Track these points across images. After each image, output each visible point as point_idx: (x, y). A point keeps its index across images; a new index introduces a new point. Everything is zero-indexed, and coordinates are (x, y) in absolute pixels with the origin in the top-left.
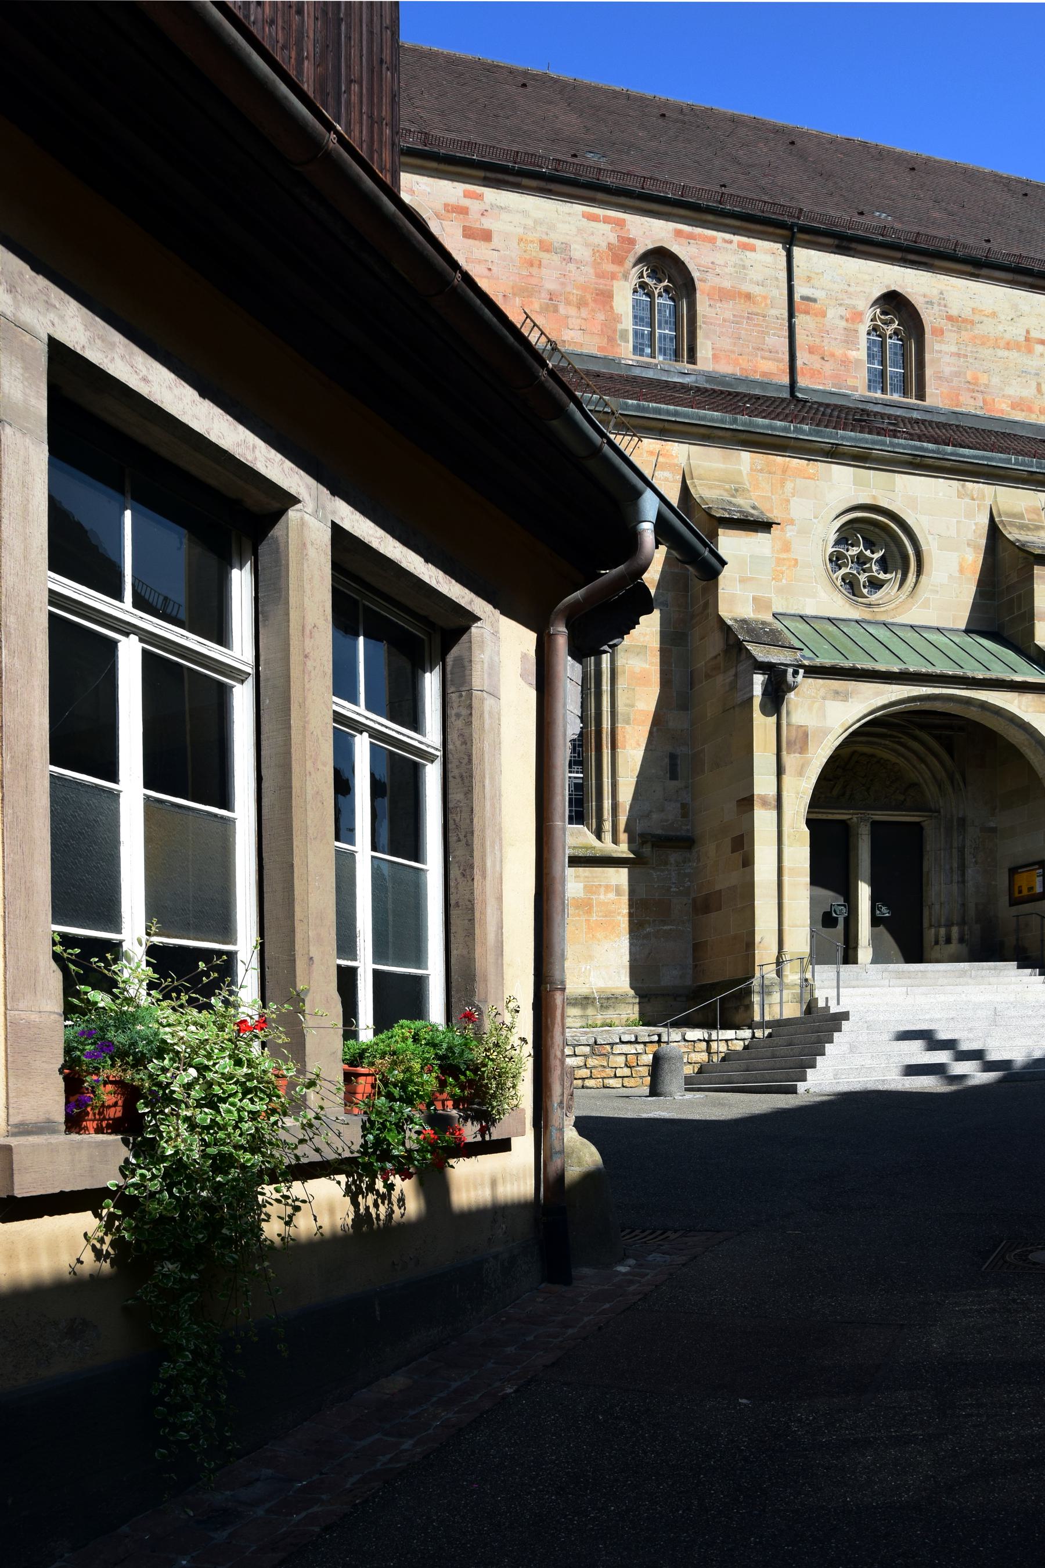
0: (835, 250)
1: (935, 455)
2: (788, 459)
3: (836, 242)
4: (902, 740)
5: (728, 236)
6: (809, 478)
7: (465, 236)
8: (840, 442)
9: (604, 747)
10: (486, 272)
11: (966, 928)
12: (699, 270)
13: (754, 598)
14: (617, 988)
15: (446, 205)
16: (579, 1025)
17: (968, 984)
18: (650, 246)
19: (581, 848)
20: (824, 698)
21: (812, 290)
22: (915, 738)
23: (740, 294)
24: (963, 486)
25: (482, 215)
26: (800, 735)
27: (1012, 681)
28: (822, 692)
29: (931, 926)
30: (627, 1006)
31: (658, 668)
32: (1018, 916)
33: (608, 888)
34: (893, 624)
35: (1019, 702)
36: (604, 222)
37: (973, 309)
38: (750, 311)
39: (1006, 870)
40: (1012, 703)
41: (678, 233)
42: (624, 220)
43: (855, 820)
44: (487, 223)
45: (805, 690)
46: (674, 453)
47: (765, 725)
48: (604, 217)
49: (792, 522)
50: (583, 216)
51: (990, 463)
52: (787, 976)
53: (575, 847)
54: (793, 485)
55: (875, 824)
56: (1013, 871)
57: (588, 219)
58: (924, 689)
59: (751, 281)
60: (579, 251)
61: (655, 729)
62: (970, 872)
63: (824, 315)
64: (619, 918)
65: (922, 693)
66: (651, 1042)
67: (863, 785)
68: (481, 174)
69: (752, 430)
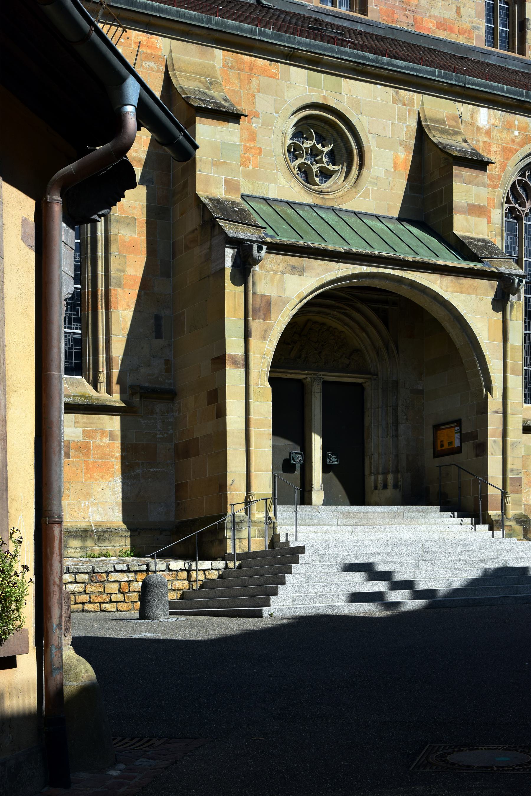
1: (374, 64)
2: (254, 59)
4: (347, 311)
6: (271, 77)
8: (297, 47)
9: (100, 307)
11: (399, 476)
13: (226, 181)
14: (112, 522)
16: (79, 555)
17: (400, 524)
19: (80, 396)
20: (283, 272)
22: (358, 310)
24: (397, 93)
26: (264, 303)
28: (282, 266)
29: (371, 473)
30: (120, 538)
31: (145, 238)
32: (440, 466)
34: (340, 210)
35: (441, 282)
39: (431, 427)
40: (435, 283)
43: (309, 379)
45: (268, 264)
47: (235, 293)
49: (257, 115)
52: (254, 514)
53: (74, 396)
54: (258, 82)
56: (436, 428)
58: (365, 268)
61: (142, 293)
62: (402, 428)
65: (363, 271)
66: (141, 571)
67: (316, 350)
69: (225, 30)
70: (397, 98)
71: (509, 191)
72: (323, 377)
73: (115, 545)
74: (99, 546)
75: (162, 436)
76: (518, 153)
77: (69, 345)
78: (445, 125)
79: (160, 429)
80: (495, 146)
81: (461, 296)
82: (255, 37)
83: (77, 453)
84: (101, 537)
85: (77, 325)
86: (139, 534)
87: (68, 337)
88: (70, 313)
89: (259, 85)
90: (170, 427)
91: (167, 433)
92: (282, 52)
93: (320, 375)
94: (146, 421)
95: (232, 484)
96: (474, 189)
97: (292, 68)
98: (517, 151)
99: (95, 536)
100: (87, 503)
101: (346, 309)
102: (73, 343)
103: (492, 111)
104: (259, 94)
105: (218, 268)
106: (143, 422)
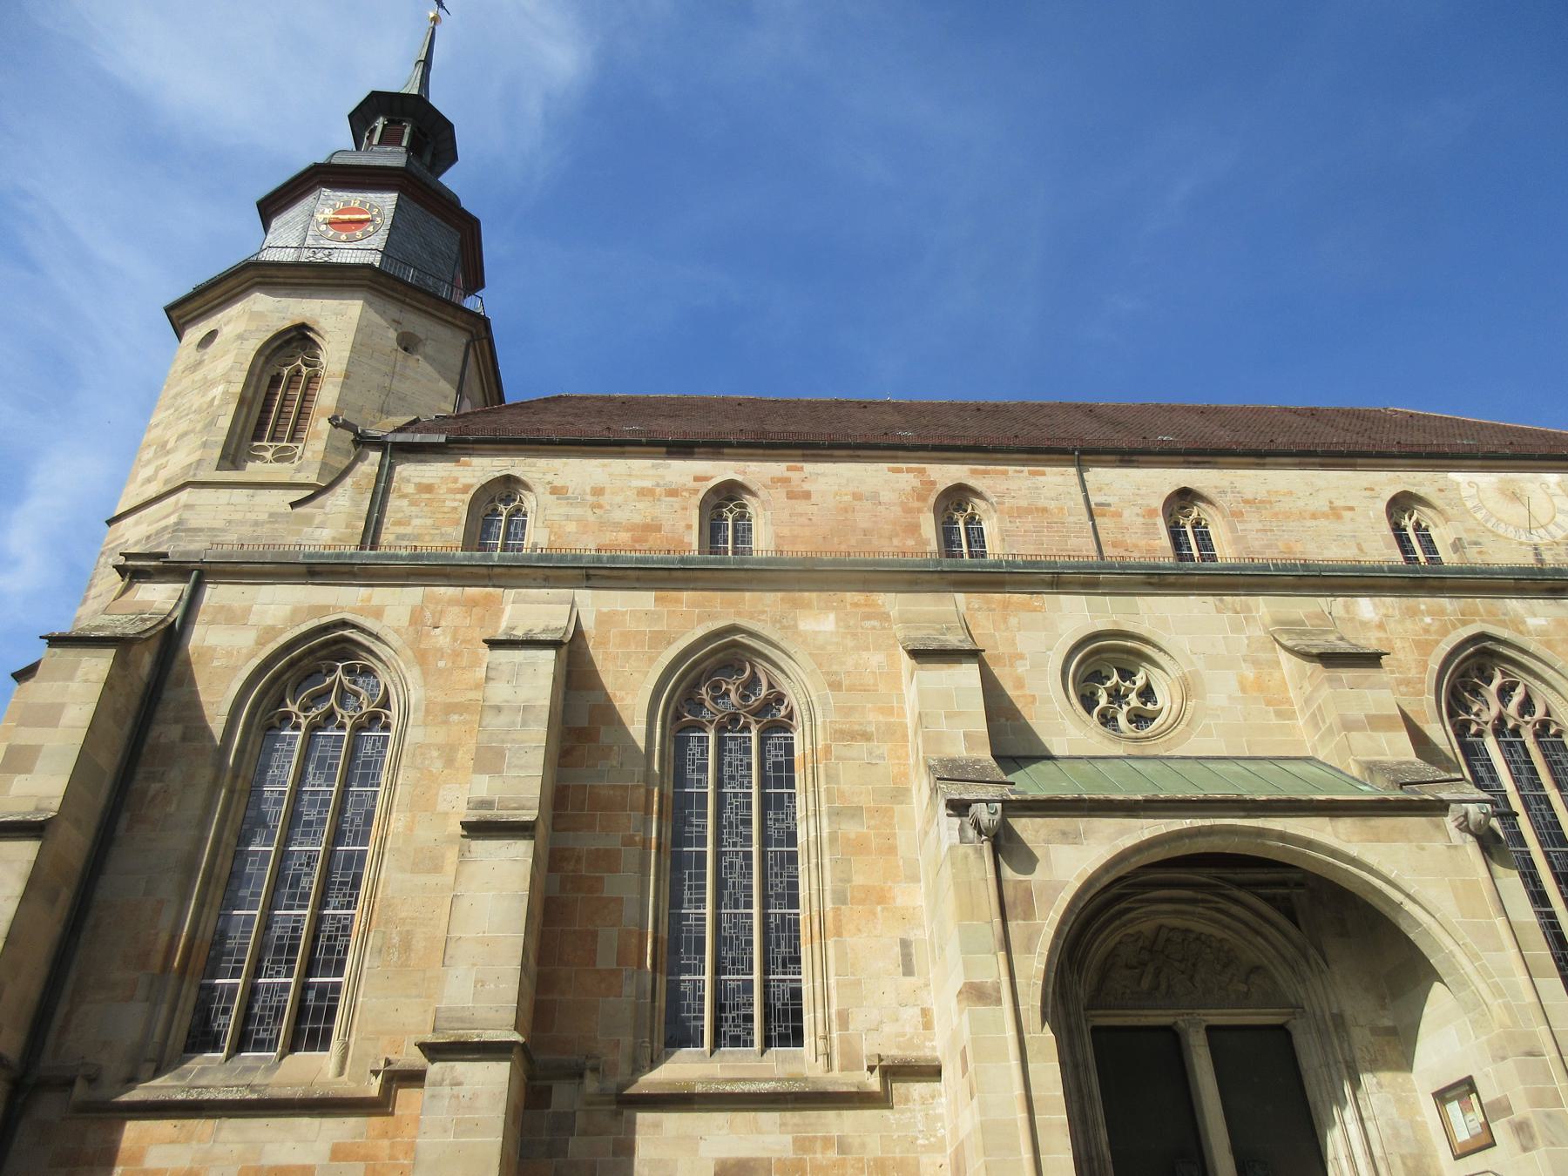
0: (1118, 464)
1: (1175, 572)
2: (1008, 595)
3: (1118, 457)
4: (1220, 906)
5: (1018, 468)
6: (1035, 611)
7: (788, 498)
10: (807, 522)
15: (772, 479)
19: (788, 1080)
20: (1048, 842)
22: (1237, 901)
23: (1037, 509)
24: (1221, 601)
25: (803, 481)
27: (1311, 801)
33: (827, 1142)
36: (907, 472)
37: (1268, 492)
38: (1049, 521)
41: (974, 472)
42: (925, 468)
44: (806, 487)
46: (880, 602)
49: (1021, 657)
51: (1243, 573)
54: (1017, 619)
55: (1211, 1030)
58: (1188, 821)
59: (1046, 498)
60: (886, 496)
63: (1120, 515)
67: (1183, 973)
68: (800, 452)
70: (1223, 607)
71: (1452, 702)
72: (1205, 1018)
75: (927, 1142)
76: (1442, 645)
78: (1306, 626)
79: (921, 1128)
80: (1398, 641)
81: (1381, 847)
89: (1019, 623)
90: (939, 1125)
91: (935, 1136)
94: (897, 1116)
96: (1369, 694)
98: (1437, 642)
104: (1021, 632)
106: (892, 1117)
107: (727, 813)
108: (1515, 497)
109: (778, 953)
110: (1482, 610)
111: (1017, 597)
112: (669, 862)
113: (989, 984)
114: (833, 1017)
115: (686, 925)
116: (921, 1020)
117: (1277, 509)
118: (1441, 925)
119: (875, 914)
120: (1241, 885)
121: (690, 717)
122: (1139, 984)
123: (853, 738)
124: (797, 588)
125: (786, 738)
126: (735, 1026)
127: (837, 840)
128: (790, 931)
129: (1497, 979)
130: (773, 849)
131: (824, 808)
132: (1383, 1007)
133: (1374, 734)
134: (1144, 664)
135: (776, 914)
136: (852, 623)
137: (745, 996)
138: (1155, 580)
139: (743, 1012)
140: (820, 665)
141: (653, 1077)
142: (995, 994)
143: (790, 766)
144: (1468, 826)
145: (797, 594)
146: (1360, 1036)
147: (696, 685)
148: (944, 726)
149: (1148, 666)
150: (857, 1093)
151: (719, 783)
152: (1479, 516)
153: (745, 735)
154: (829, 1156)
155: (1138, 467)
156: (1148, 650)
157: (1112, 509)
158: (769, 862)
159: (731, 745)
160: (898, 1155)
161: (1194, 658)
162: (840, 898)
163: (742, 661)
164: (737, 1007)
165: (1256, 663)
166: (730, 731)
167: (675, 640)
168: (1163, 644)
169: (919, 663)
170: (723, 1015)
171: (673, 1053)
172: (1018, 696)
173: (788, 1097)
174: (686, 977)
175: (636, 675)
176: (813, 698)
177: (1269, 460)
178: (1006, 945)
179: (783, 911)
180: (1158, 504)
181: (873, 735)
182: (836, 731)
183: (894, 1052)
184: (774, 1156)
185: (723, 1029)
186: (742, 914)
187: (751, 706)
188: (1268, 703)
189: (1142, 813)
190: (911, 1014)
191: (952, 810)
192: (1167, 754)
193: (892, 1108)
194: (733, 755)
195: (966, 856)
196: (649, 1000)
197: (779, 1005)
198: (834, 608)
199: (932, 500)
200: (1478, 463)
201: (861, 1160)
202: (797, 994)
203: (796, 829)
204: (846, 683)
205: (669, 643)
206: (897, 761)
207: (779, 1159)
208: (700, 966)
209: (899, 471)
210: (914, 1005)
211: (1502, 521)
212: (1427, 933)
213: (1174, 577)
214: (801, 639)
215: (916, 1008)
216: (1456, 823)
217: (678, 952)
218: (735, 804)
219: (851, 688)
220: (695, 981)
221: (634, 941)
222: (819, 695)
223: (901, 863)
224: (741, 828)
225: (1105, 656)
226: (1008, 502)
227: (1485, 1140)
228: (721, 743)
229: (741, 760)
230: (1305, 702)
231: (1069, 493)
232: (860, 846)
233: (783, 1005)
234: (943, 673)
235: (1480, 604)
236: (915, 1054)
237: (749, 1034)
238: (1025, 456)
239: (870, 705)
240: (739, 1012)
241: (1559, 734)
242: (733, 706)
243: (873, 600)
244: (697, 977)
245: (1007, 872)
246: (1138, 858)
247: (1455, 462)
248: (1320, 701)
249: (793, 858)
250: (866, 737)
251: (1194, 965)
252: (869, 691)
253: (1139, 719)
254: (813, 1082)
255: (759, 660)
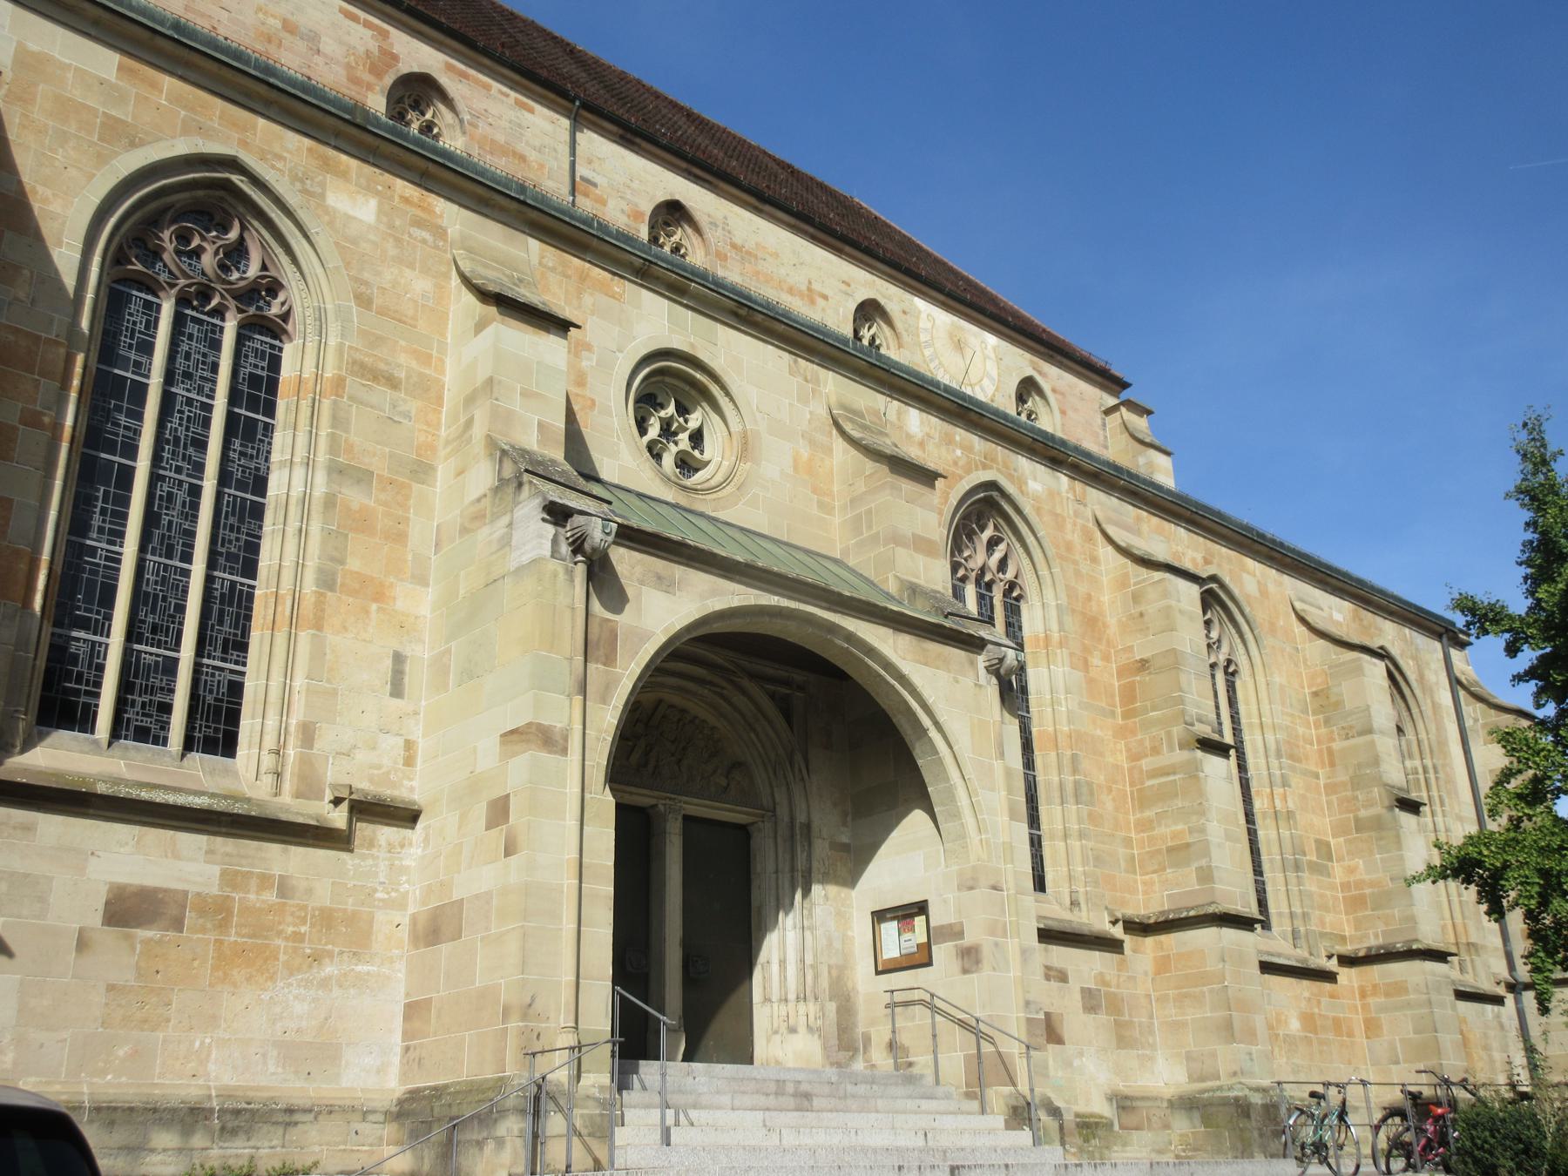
1: (765, 311)
2: (588, 265)
3: (621, 132)
4: (725, 692)
5: (505, 89)
6: (613, 297)
8: (654, 260)
12: (470, 114)
13: (541, 425)
14: (258, 1089)
18: (416, 69)
19: (225, 797)
20: (642, 583)
21: (595, 175)
22: (744, 692)
23: (515, 153)
30: (272, 1129)
32: (892, 992)
33: (265, 881)
36: (365, 26)
41: (449, 67)
42: (388, 32)
46: (437, 210)
48: (365, 20)
50: (340, 11)
55: (688, 819)
57: (346, 16)
58: (776, 598)
59: (527, 143)
60: (328, 45)
64: (280, 942)
67: (673, 755)
69: (546, 209)
73: (259, 1144)
74: (221, 1148)
75: (386, 896)
76: (964, 482)
77: (218, 694)
79: (382, 880)
82: (591, 231)
83: (201, 921)
84: (229, 1125)
85: (238, 656)
86: (316, 1118)
87: (217, 678)
88: (228, 629)
89: (593, 305)
90: (404, 878)
91: (397, 890)
92: (631, 263)
93: (680, 802)
94: (357, 861)
95: (530, 1005)
97: (645, 292)
98: (961, 478)
99: (216, 1121)
100: (208, 1041)
101: (723, 688)
102: (225, 690)
103: (925, 415)
104: (594, 317)
105: (524, 559)
106: (350, 862)
107: (175, 421)
108: (959, 346)
109: (219, 631)
110: (1000, 459)
111: (597, 272)
112: (78, 466)
113: (557, 729)
114: (292, 729)
115: (88, 563)
116: (403, 753)
117: (760, 267)
118: (955, 757)
119: (367, 612)
120: (753, 676)
121: (139, 267)
122: (628, 758)
123: (375, 379)
124: (333, 144)
125: (272, 347)
126: (143, 715)
127: (334, 505)
128: (239, 606)
129: (985, 816)
130: (232, 491)
131: (322, 457)
132: (844, 824)
133: (915, 555)
134: (704, 404)
135: (223, 579)
136: (398, 223)
137: (165, 678)
138: (743, 312)
139: (158, 698)
140: (348, 265)
141: (30, 762)
142: (561, 741)
143: (273, 386)
144: (998, 669)
145: (331, 152)
146: (821, 848)
147: (154, 222)
148: (516, 404)
149: (708, 408)
150: (317, 827)
151: (169, 378)
152: (927, 352)
153: (214, 321)
154: (264, 898)
155: (637, 153)
156: (715, 389)
157: (597, 192)
158: (225, 509)
159: (192, 328)
160: (350, 908)
161: (757, 414)
162: (327, 581)
163: (230, 215)
164: (151, 690)
165: (812, 443)
166: (194, 308)
167: (142, 144)
168: (733, 390)
169: (501, 314)
170: (129, 696)
171: (48, 734)
172: (577, 395)
173: (224, 818)
174: (82, 634)
175: (73, 172)
176: (328, 306)
177: (767, 208)
178: (583, 689)
179: (234, 578)
180: (647, 208)
181: (401, 383)
182: (354, 362)
183: (367, 786)
184: (193, 889)
185: (126, 715)
186: (176, 567)
187: (233, 284)
188: (815, 491)
189: (738, 577)
190: (391, 746)
191: (548, 514)
192: (713, 514)
193: (351, 851)
194: (194, 344)
195: (555, 575)
196: (32, 655)
197: (210, 699)
198: (378, 193)
199: (389, 80)
200: (942, 297)
201: (304, 908)
202: (236, 689)
203: (268, 474)
204: (377, 302)
205: (133, 145)
206: (425, 428)
207: (198, 894)
208: (103, 624)
209: (355, 19)
210: (397, 734)
211: (943, 366)
212: (940, 762)
213: (763, 317)
214: (326, 218)
215: (398, 738)
216: (987, 664)
217: (72, 597)
218: (187, 413)
219: (382, 312)
220: (94, 643)
221: (23, 566)
222: (339, 306)
223: (410, 557)
224: (191, 450)
225: (668, 379)
226: (483, 128)
227: (925, 960)
228: (179, 321)
229: (205, 355)
230: (851, 501)
231: (555, 150)
232: (362, 522)
233: (216, 700)
234: (527, 337)
235: (1000, 452)
236: (388, 792)
237: (163, 728)
238: (517, 77)
239: (402, 343)
240: (153, 698)
241: (1018, 599)
242: (204, 274)
243: (429, 204)
244: (97, 638)
245: (596, 606)
246: (719, 624)
247: (925, 289)
248: (873, 505)
249: (258, 512)
250: (393, 383)
251: (684, 749)
252: (404, 323)
253: (686, 465)
254: (258, 805)
255: (256, 223)
